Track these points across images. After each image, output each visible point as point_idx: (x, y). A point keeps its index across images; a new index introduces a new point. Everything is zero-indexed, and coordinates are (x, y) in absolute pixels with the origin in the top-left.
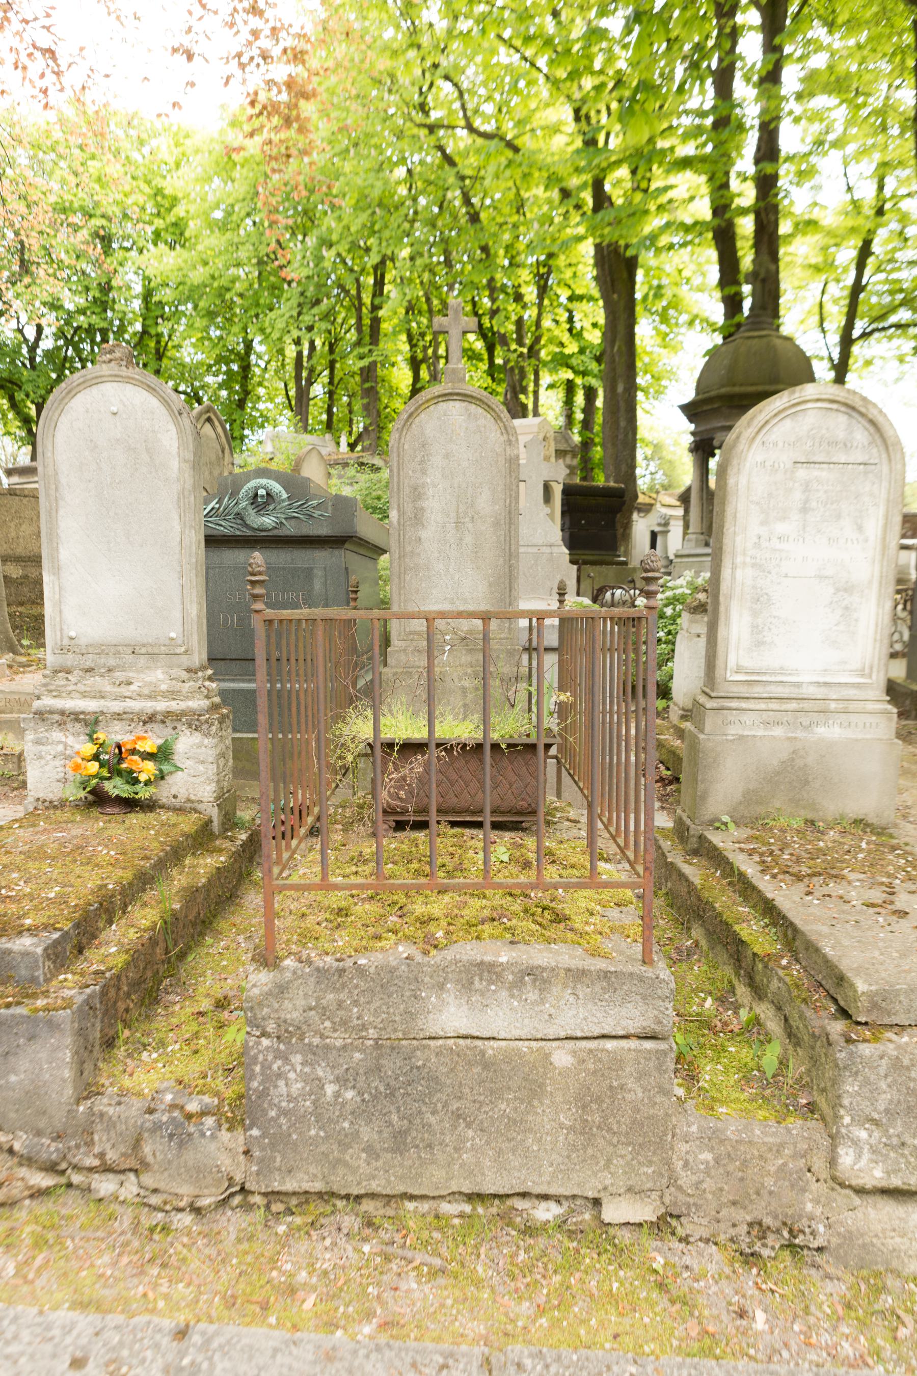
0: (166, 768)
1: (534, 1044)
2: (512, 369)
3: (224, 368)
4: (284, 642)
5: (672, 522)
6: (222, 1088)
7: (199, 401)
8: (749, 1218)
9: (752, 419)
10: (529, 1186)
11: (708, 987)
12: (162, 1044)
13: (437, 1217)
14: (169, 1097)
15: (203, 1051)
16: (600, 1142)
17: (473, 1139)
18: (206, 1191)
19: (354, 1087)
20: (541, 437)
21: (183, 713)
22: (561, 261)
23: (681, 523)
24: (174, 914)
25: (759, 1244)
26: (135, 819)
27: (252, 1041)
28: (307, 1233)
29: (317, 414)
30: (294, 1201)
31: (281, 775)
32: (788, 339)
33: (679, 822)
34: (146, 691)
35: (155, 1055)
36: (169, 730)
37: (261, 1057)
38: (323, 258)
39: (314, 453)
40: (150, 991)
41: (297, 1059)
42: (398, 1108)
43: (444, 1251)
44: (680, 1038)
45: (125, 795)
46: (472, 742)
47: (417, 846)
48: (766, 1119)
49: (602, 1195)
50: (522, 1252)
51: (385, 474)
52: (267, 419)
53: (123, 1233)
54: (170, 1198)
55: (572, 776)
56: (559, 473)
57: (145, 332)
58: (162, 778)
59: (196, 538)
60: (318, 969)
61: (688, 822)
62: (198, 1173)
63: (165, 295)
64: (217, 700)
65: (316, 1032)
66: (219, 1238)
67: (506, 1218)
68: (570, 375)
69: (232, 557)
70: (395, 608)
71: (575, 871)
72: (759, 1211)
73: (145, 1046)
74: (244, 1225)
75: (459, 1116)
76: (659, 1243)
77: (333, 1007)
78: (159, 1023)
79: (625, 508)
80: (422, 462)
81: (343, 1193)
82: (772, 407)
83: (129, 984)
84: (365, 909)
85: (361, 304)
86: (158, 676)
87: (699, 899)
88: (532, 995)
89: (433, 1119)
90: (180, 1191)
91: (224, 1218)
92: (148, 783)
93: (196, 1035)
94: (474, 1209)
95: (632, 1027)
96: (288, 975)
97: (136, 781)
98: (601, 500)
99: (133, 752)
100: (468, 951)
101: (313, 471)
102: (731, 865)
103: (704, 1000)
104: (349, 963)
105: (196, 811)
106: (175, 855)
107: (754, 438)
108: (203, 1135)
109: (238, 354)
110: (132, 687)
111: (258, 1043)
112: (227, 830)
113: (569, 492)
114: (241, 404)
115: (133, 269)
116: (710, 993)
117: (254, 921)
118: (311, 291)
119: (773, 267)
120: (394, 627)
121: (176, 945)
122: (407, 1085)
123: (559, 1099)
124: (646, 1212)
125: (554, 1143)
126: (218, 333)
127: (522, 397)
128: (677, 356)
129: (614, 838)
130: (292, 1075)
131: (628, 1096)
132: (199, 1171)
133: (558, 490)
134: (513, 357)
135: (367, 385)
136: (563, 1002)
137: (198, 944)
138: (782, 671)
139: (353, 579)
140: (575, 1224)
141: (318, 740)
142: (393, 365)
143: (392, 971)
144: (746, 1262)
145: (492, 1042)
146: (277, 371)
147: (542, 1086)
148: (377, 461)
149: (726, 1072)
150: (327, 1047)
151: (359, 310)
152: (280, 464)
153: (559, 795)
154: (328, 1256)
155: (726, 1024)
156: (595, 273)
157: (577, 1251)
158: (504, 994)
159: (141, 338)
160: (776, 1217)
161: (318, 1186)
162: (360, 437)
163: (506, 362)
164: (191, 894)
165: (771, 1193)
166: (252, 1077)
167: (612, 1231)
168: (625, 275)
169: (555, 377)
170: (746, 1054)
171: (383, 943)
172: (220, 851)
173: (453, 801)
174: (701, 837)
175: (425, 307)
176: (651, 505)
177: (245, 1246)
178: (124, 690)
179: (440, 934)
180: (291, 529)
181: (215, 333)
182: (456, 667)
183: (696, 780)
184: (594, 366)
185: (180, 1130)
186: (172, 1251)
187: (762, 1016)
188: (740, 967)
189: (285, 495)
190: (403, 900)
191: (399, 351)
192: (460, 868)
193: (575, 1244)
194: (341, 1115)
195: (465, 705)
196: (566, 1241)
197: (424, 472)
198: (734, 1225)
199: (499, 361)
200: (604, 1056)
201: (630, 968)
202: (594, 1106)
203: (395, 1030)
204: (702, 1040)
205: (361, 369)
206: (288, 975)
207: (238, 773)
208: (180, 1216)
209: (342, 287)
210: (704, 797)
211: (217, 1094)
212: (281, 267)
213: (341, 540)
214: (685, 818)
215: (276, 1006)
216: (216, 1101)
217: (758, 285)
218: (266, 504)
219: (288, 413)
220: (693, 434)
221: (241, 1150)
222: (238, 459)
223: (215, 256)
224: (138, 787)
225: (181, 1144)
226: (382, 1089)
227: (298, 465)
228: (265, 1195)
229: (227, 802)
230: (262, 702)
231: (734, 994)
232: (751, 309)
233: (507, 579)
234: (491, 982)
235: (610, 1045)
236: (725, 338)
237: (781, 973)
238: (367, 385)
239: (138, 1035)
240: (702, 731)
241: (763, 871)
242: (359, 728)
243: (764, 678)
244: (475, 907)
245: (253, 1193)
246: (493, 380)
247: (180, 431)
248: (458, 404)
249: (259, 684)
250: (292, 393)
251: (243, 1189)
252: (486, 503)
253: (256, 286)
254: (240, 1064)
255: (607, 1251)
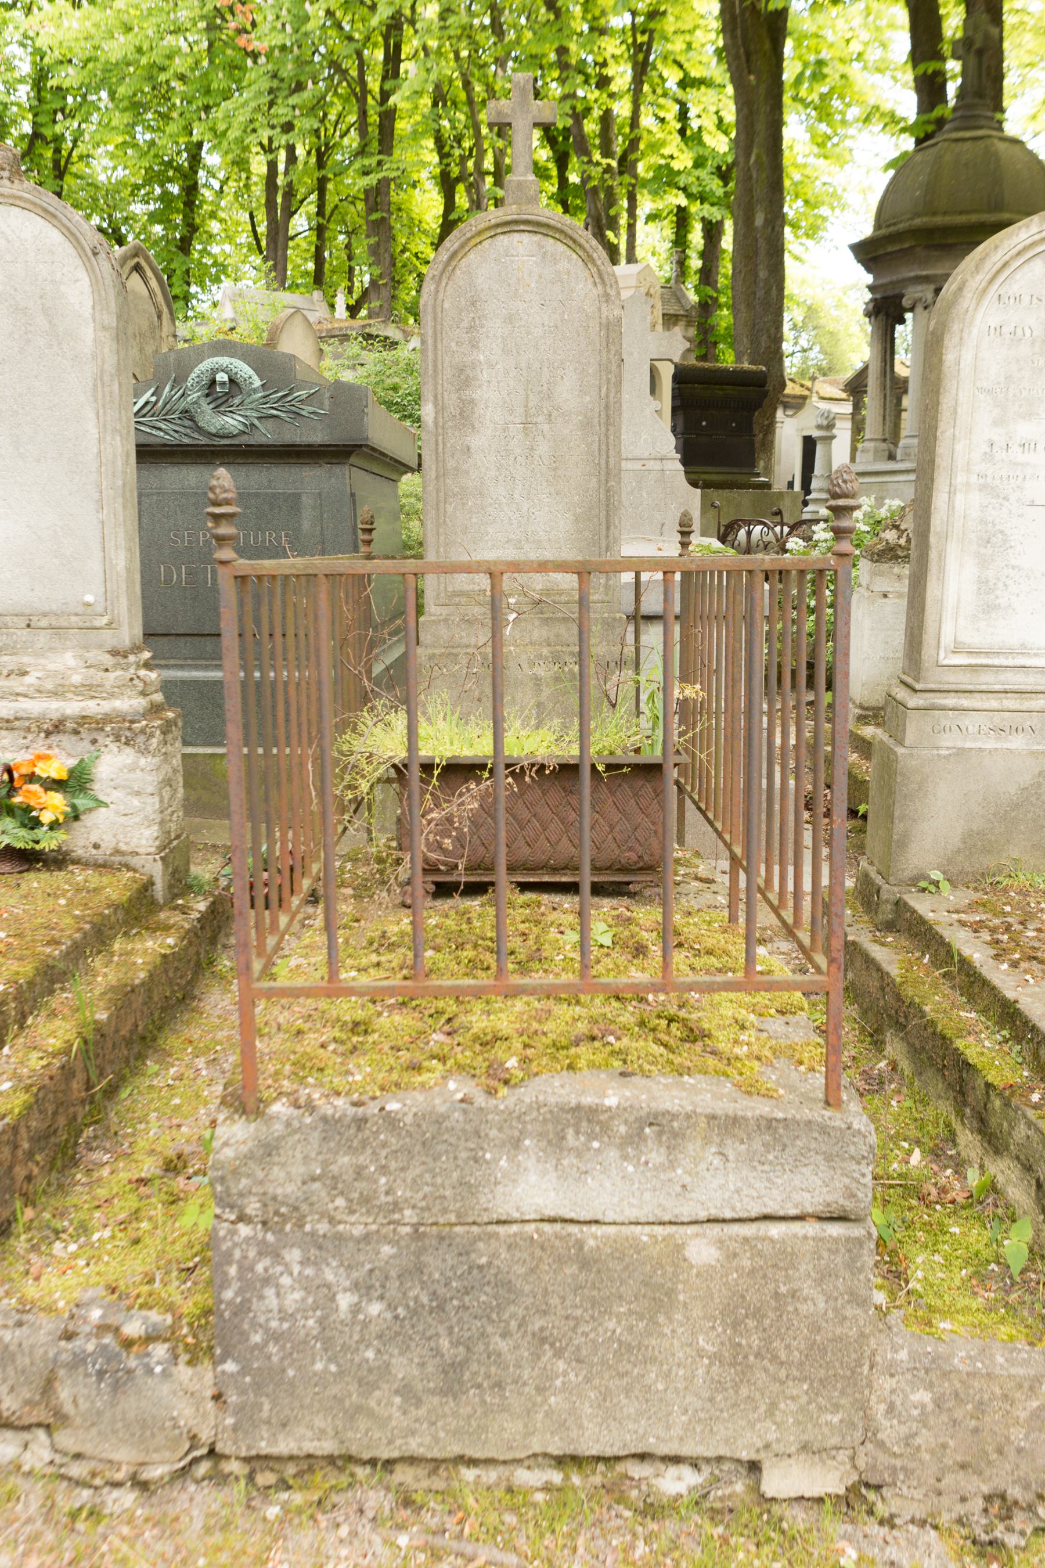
0: (81, 802)
1: (658, 1230)
2: (595, 190)
3: (158, 191)
4: (265, 610)
5: (839, 424)
6: (177, 1298)
7: (121, 241)
8: (986, 1489)
9: (982, 260)
10: (652, 1444)
11: (913, 1133)
12: (84, 1229)
13: (510, 1490)
14: (96, 1314)
15: (147, 1240)
16: (760, 1376)
17: (565, 1374)
18: (156, 1457)
19: (382, 1298)
20: (643, 290)
21: (107, 719)
22: (669, 24)
23: (849, 425)
24: (99, 1029)
25: (1001, 1527)
26: (36, 881)
27: (223, 1229)
28: (312, 1517)
29: (299, 260)
30: (291, 1469)
31: (262, 813)
32: (1016, 142)
33: (865, 880)
34: (49, 685)
35: (73, 1247)
36: (86, 745)
37: (237, 1254)
38: (307, 18)
39: (298, 319)
40: (63, 1148)
41: (293, 1256)
42: (450, 1330)
43: (521, 1542)
44: (877, 1215)
45: (19, 845)
46: (552, 763)
47: (469, 921)
48: (1011, 1338)
49: (762, 1456)
50: (640, 1544)
51: (404, 353)
52: (223, 268)
53: (29, 1520)
54: (100, 1467)
55: (704, 813)
56: (676, 346)
57: (36, 135)
58: (76, 818)
59: (121, 450)
60: (324, 1119)
61: (879, 880)
62: (143, 1430)
63: (68, 77)
64: (159, 697)
65: (322, 1215)
66: (177, 1526)
67: (615, 1491)
68: (683, 201)
69: (185, 477)
70: (431, 557)
71: (713, 960)
72: (1002, 1477)
73: (57, 1232)
74: (214, 1507)
75: (543, 1340)
76: (849, 1528)
77: (349, 1176)
78: (79, 1196)
79: (766, 401)
80: (471, 328)
81: (366, 1456)
82: (1015, 240)
83: (31, 1139)
84: (393, 1022)
85: (365, 91)
86: (68, 662)
87: (899, 998)
88: (656, 1156)
89: (503, 1345)
90: (116, 1456)
91: (184, 1496)
92: (54, 826)
93: (136, 1215)
94: (567, 1478)
95: (811, 1203)
96: (278, 1128)
97: (36, 823)
98: (730, 390)
99: (31, 778)
100: (556, 1088)
101: (296, 344)
102: (942, 942)
103: (909, 1153)
104: (373, 1109)
105: (129, 868)
106: (98, 936)
107: (985, 290)
108: (150, 1371)
109: (178, 169)
110: (28, 679)
111: (233, 1233)
112: (176, 896)
113: (681, 377)
114: (184, 246)
115: (17, 37)
116: (918, 1142)
117: (220, 1035)
118: (288, 69)
119: (994, 31)
120: (430, 584)
121: (101, 1075)
122: (462, 1294)
123: (697, 1312)
124: (830, 1481)
125: (690, 1379)
126: (148, 136)
127: (610, 234)
128: (845, 172)
129: (776, 910)
130: (286, 1281)
131: (803, 1308)
132: (144, 1425)
133: (667, 372)
134: (596, 172)
135: (374, 216)
136: (703, 1166)
137: (136, 1072)
138: (1024, 650)
139: (364, 511)
140: (721, 1499)
141: (320, 760)
142: (414, 186)
143: (439, 1120)
144: (982, 1555)
145: (594, 1228)
146: (236, 196)
147: (671, 1293)
148: (392, 332)
149: (947, 1266)
150: (340, 1238)
151: (362, 100)
152: (246, 334)
153: (681, 841)
154: (344, 1552)
155: (943, 1190)
156: (721, 43)
157: (725, 1540)
158: (613, 1154)
159: (31, 144)
160: (1027, 1487)
161: (327, 1447)
162: (365, 293)
163: (585, 180)
164: (124, 997)
165: (1019, 1451)
166: (225, 1284)
167: (776, 1510)
168: (767, 46)
169: (660, 205)
170: (977, 1237)
171: (425, 1077)
172: (166, 928)
173: (524, 852)
174: (899, 905)
175: (463, 96)
176: (804, 398)
177: (217, 1538)
178: (15, 684)
179: (512, 1062)
180: (267, 435)
181: (143, 136)
182: (526, 644)
183: (891, 816)
184: (715, 186)
185: (114, 1365)
186: (105, 1548)
187: (1000, 1178)
188: (965, 1104)
189: (257, 383)
190: (452, 1008)
191: (424, 164)
192: (537, 956)
193: (720, 1530)
194: (362, 1340)
195: (539, 705)
196: (707, 1526)
197: (474, 345)
198: (963, 1500)
199: (574, 178)
200: (766, 1248)
201: (806, 1113)
202: (751, 1323)
203: (445, 1211)
204: (909, 1215)
205: (366, 192)
206: (278, 1128)
207: (191, 807)
208: (116, 1493)
209: (335, 65)
210: (903, 843)
211: (170, 1308)
212: (241, 31)
213: (335, 452)
214: (873, 874)
215: (260, 1175)
216: (169, 1319)
217: (972, 60)
218: (229, 395)
219: (257, 260)
220: (871, 288)
221: (209, 1393)
222: (183, 329)
223: (144, 17)
224: (40, 832)
225: (116, 1387)
226: (425, 1300)
227: (274, 335)
228: (247, 1460)
229: (176, 853)
230: (233, 704)
231: (955, 1144)
232: (961, 94)
233: (604, 511)
234: (591, 1136)
235: (775, 1230)
236: (919, 142)
237: (1031, 1114)
238: (374, 216)
239: (47, 1215)
240: (901, 743)
241: (996, 957)
242: (383, 739)
243: (996, 661)
244: (563, 1019)
245: (228, 1457)
246: (566, 210)
247: (96, 282)
248: (526, 238)
249: (227, 673)
250: (262, 229)
251: (212, 1452)
252: (571, 394)
253: (205, 63)
254: (205, 1261)
255: (769, 1540)
